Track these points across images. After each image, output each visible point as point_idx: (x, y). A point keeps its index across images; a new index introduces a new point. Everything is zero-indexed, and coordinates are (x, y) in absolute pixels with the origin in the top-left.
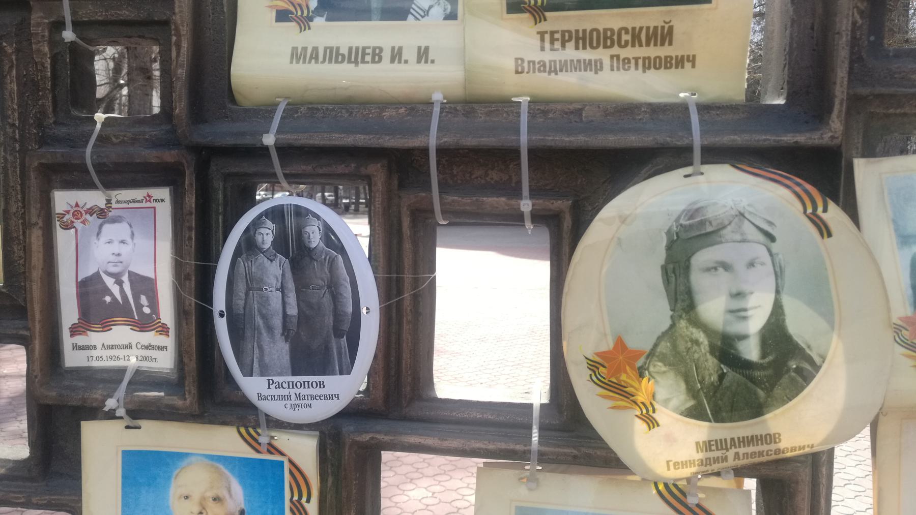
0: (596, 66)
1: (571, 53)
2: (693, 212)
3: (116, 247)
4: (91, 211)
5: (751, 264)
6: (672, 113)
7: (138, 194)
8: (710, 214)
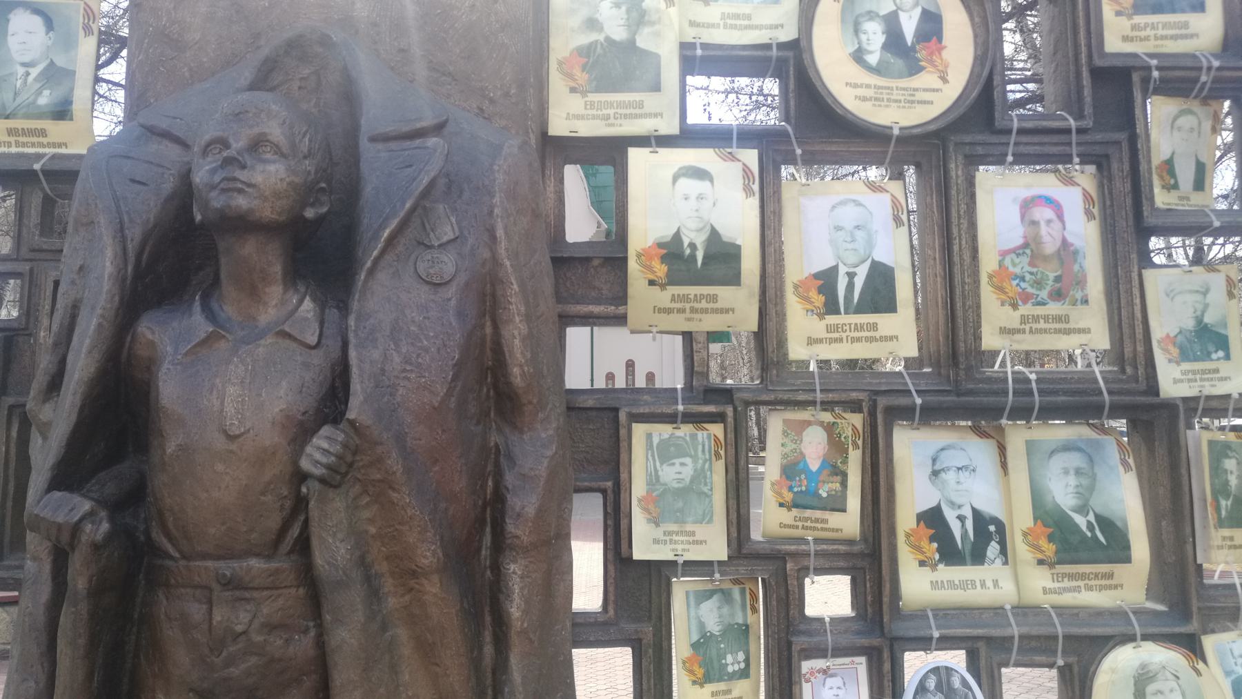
0: (1077, 589)
1: (1067, 583)
2: (1143, 666)
3: (835, 691)
4: (819, 671)
5: (1171, 691)
6: (1117, 614)
7: (847, 660)
8: (1151, 668)
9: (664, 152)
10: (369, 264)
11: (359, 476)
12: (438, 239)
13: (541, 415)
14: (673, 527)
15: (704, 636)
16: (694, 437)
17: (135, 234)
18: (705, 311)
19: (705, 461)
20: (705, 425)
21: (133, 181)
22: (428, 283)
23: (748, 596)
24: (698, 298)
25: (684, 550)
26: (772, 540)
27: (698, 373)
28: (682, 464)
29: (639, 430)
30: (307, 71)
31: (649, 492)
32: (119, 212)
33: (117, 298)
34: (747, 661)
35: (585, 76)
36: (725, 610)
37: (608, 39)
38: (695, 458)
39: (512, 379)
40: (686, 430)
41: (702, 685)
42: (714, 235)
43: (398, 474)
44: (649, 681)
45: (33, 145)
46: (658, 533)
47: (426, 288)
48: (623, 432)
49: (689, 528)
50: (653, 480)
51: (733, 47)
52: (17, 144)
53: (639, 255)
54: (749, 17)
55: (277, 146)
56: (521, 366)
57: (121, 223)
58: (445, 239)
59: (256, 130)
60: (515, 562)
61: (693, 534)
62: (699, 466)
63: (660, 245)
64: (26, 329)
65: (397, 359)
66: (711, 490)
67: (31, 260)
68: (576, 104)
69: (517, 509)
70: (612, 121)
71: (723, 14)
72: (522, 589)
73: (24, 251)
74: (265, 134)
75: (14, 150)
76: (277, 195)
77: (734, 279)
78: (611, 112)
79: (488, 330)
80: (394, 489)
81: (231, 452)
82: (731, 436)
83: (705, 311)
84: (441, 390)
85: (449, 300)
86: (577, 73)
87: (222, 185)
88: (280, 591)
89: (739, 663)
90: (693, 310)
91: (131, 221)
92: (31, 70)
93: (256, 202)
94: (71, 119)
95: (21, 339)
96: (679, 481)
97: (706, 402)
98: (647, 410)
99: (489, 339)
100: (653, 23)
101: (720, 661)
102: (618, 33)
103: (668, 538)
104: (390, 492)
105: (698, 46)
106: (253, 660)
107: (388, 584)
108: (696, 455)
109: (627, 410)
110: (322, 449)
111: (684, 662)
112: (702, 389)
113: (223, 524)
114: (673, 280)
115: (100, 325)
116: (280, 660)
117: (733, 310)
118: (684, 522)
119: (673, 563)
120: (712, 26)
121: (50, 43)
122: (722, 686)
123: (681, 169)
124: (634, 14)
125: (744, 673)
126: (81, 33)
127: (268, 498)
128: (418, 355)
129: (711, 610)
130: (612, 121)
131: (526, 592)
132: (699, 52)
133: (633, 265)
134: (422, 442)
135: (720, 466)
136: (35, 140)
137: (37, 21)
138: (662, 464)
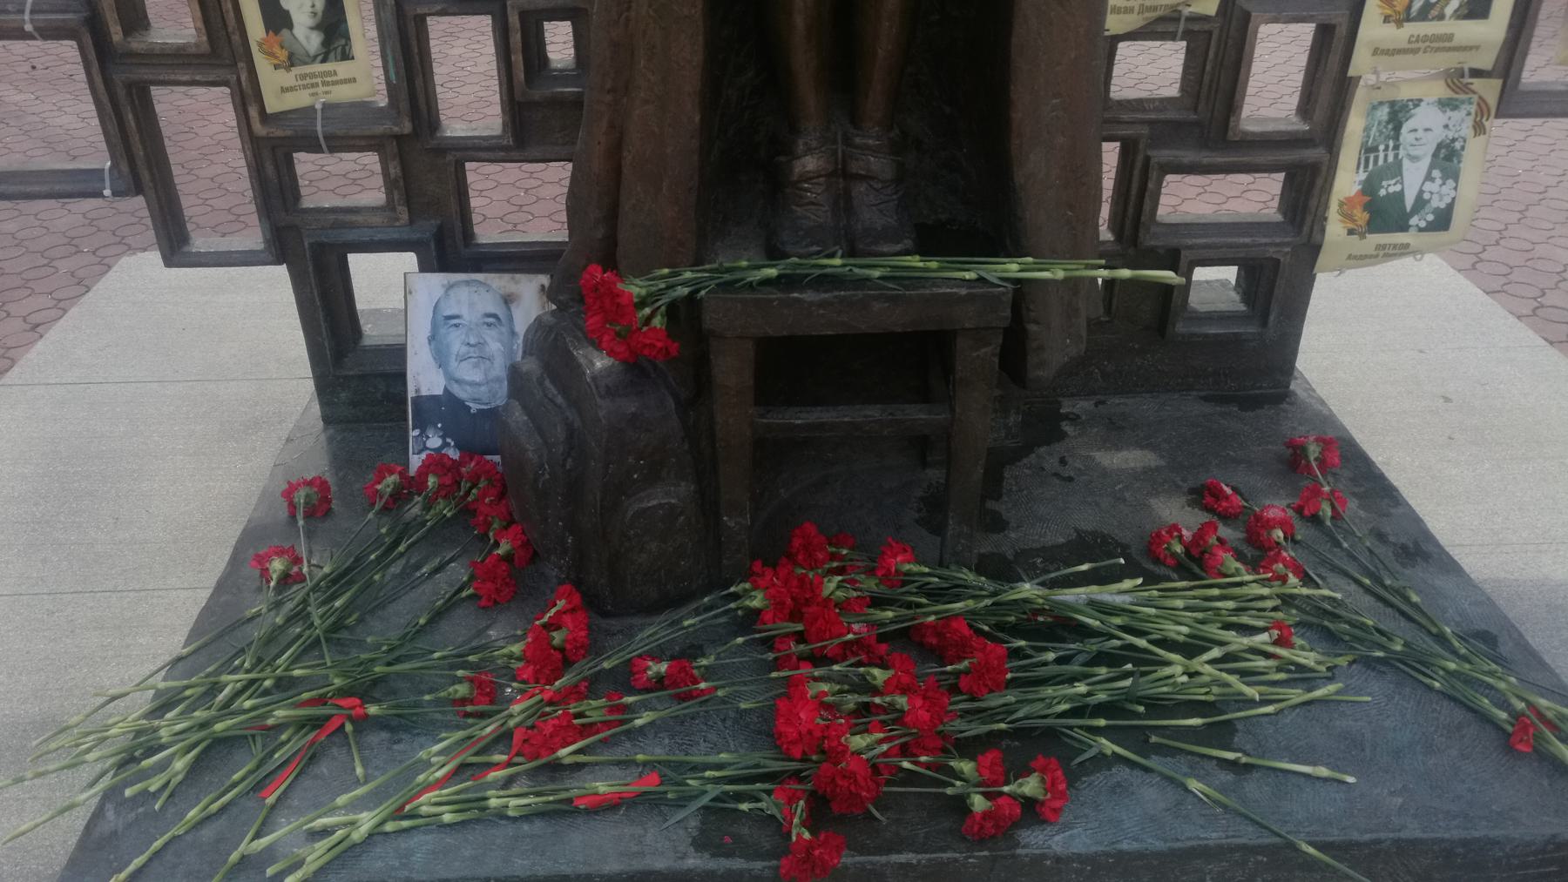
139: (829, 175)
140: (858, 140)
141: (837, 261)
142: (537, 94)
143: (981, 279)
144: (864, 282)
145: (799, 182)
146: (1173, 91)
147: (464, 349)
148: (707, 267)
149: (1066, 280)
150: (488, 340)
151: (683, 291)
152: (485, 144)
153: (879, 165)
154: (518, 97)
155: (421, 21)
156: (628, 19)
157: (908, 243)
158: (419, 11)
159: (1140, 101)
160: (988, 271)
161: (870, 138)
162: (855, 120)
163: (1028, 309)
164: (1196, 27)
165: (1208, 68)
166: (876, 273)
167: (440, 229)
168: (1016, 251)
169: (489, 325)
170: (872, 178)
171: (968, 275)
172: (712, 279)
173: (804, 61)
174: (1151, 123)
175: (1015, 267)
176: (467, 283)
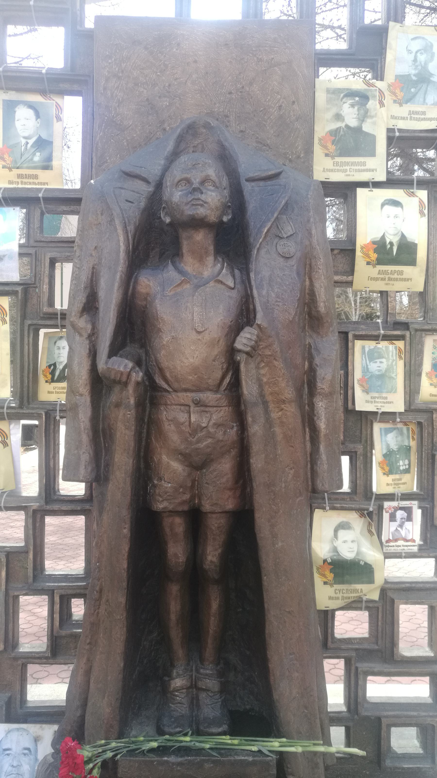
9: (377, 192)
10: (258, 246)
11: (260, 353)
12: (286, 234)
13: (331, 329)
14: (376, 395)
15: (389, 451)
16: (387, 348)
17: (131, 228)
18: (396, 280)
19: (393, 360)
20: (394, 342)
21: (127, 201)
22: (283, 257)
23: (411, 432)
24: (392, 273)
25: (381, 406)
26: (426, 403)
27: (390, 313)
28: (381, 362)
29: (358, 344)
30: (196, 142)
31: (363, 376)
32: (123, 217)
33: (127, 262)
34: (409, 465)
35: (334, 147)
36: (399, 438)
37: (347, 126)
38: (388, 359)
39: (320, 309)
40: (383, 344)
41: (388, 475)
42: (403, 236)
43: (278, 353)
44: (360, 473)
45: (30, 183)
46: (368, 397)
47: (282, 260)
48: (350, 344)
49: (384, 395)
50: (366, 370)
51: (415, 131)
52: (22, 183)
53: (362, 248)
54: (424, 113)
55: (214, 182)
56: (324, 302)
57: (125, 223)
58: (289, 234)
59: (204, 174)
60: (322, 401)
61: (386, 398)
62: (390, 363)
63: (374, 243)
64: (34, 284)
65: (273, 294)
66: (396, 376)
67: (35, 247)
68: (328, 163)
69: (323, 376)
70: (348, 173)
71: (410, 111)
72: (325, 414)
73: (32, 243)
74: (208, 176)
75: (20, 186)
76: (217, 208)
77: (413, 262)
78: (348, 168)
79: (307, 283)
80: (276, 360)
81: (199, 340)
82: (408, 347)
83: (396, 280)
84: (293, 312)
85: (293, 266)
86: (329, 145)
87: (192, 202)
88: (222, 408)
89: (405, 465)
90: (390, 279)
91: (129, 222)
92: (29, 141)
93: (209, 212)
94: (52, 169)
95: (31, 289)
96: (379, 371)
97: (395, 330)
98: (364, 333)
99: (307, 287)
100: (372, 117)
101: (396, 463)
102: (353, 123)
103: (373, 400)
104: (275, 361)
105: (396, 131)
106: (210, 440)
107: (271, 406)
108: (388, 357)
109: (353, 333)
110: (245, 339)
111: (379, 463)
112: (392, 322)
113: (196, 375)
114: (379, 262)
115: (121, 276)
116: (222, 441)
117: (411, 279)
118: (382, 392)
119: (376, 413)
120: (403, 118)
121: (38, 125)
122: (397, 476)
123: (385, 200)
124: (362, 112)
125: (407, 471)
126: (55, 120)
127: (216, 363)
128: (282, 294)
129: (393, 438)
130: (348, 173)
131: (327, 416)
132: (397, 134)
133: (358, 253)
134: (285, 338)
135: (401, 364)
136: (31, 181)
137: (30, 113)
138: (370, 362)
139: (188, 688)
140: (202, 671)
141: (188, 739)
142: (63, 633)
143: (260, 751)
144: (200, 751)
145: (173, 691)
146: (367, 635)
147: (10, 768)
148: (123, 740)
149: (303, 752)
150: (23, 763)
151: (109, 754)
152: (37, 656)
153: (212, 684)
154: (55, 634)
155: (16, 598)
156: (98, 613)
157: (225, 727)
158: (16, 594)
159: (350, 639)
160: (263, 746)
161: (208, 669)
162: (202, 660)
163: (287, 768)
164: (371, 605)
165: (380, 624)
166: (207, 746)
167: (10, 698)
168: (279, 735)
169: (25, 754)
170: (208, 690)
171: (255, 749)
172: (126, 747)
173: (176, 634)
174: (356, 650)
175: (276, 744)
176: (18, 729)
